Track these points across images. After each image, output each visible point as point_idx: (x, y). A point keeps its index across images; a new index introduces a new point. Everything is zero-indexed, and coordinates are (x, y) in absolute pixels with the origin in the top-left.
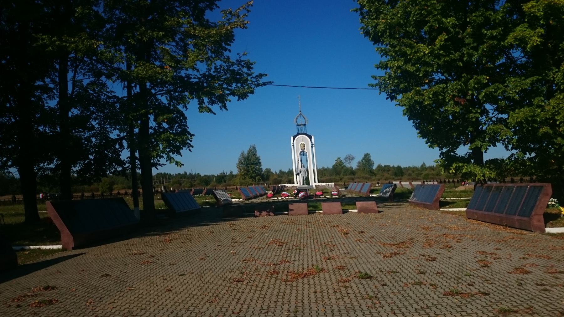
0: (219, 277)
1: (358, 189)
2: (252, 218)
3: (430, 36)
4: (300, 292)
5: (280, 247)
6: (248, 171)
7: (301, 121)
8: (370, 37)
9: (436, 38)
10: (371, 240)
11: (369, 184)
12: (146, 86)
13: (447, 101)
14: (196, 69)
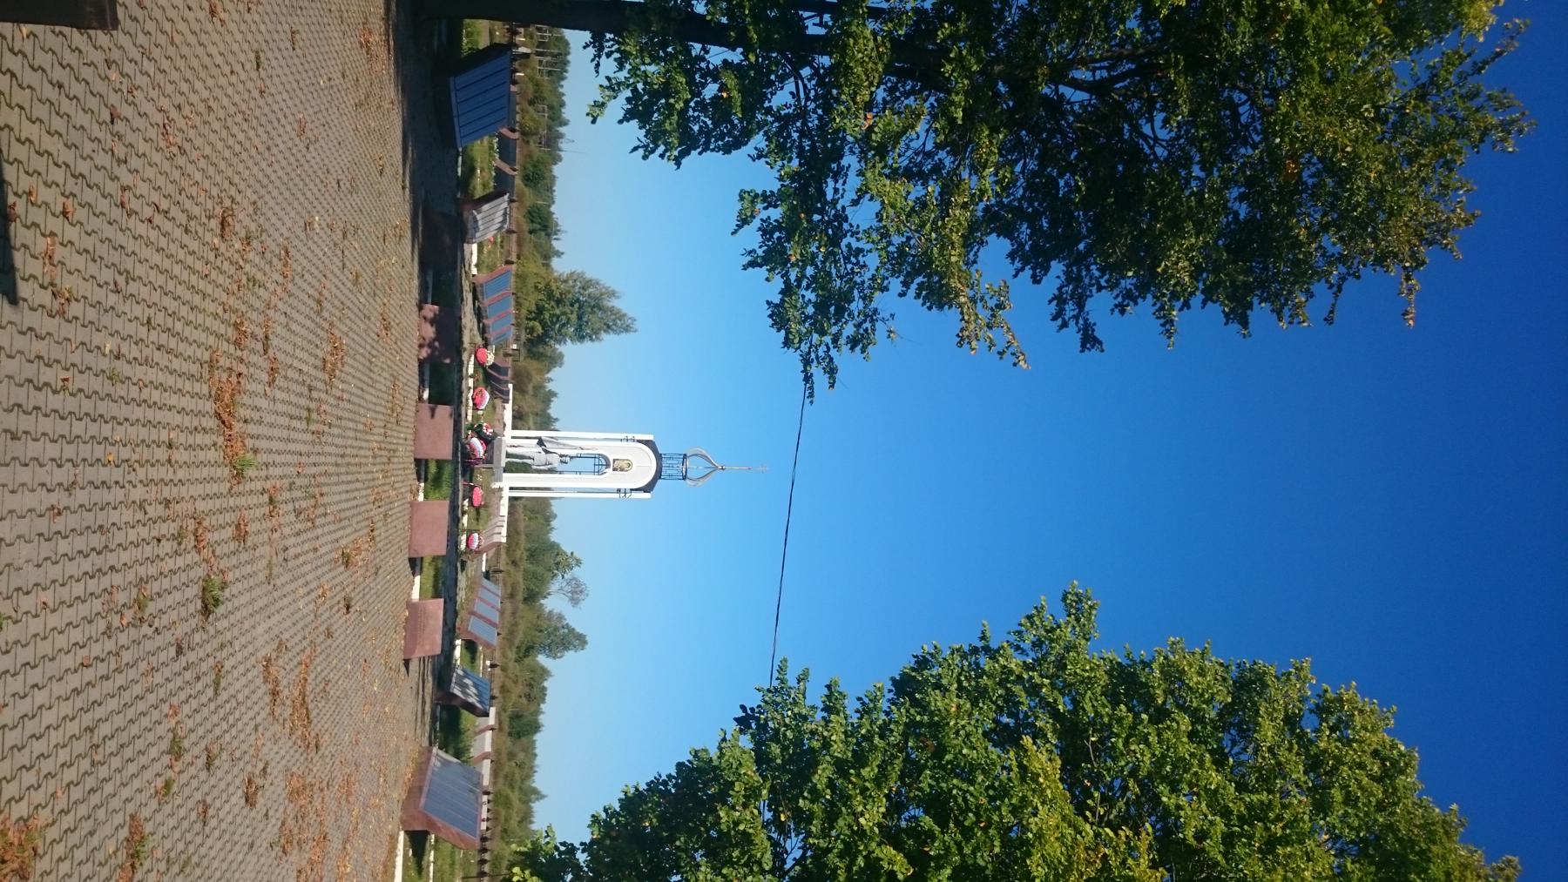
0: (241, 167)
1: (479, 607)
2: (416, 293)
3: (905, 831)
4: (174, 400)
5: (319, 363)
6: (559, 302)
7: (695, 467)
8: (913, 669)
9: (898, 846)
10: (322, 628)
11: (495, 641)
12: (822, 54)
13: (724, 871)
14: (860, 198)
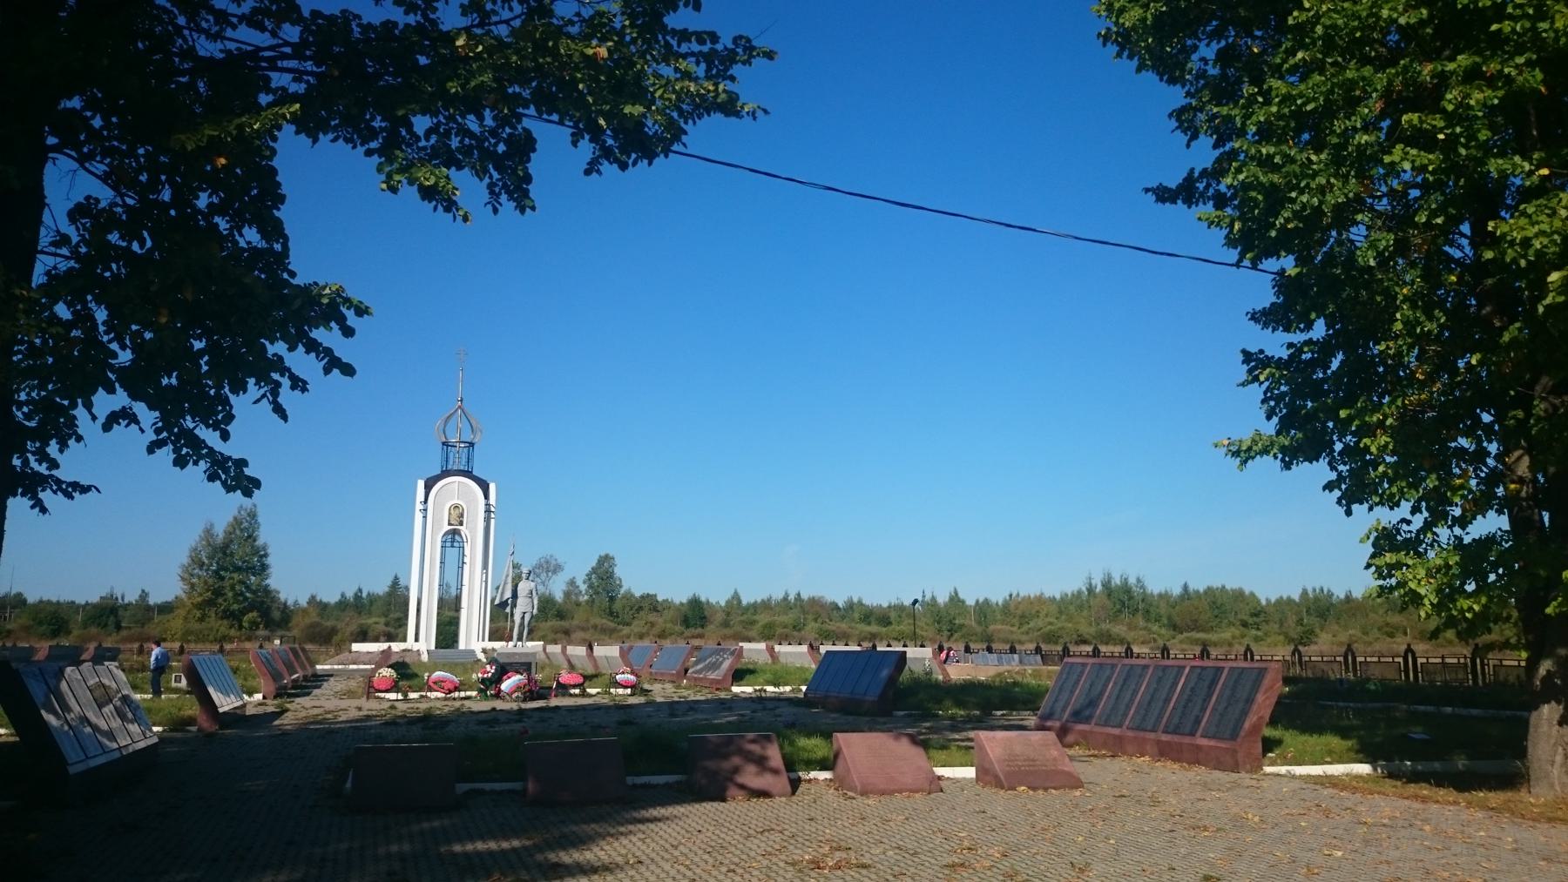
6: (218, 593)
